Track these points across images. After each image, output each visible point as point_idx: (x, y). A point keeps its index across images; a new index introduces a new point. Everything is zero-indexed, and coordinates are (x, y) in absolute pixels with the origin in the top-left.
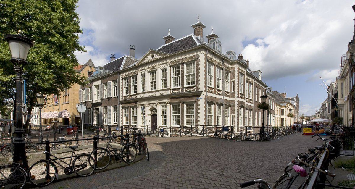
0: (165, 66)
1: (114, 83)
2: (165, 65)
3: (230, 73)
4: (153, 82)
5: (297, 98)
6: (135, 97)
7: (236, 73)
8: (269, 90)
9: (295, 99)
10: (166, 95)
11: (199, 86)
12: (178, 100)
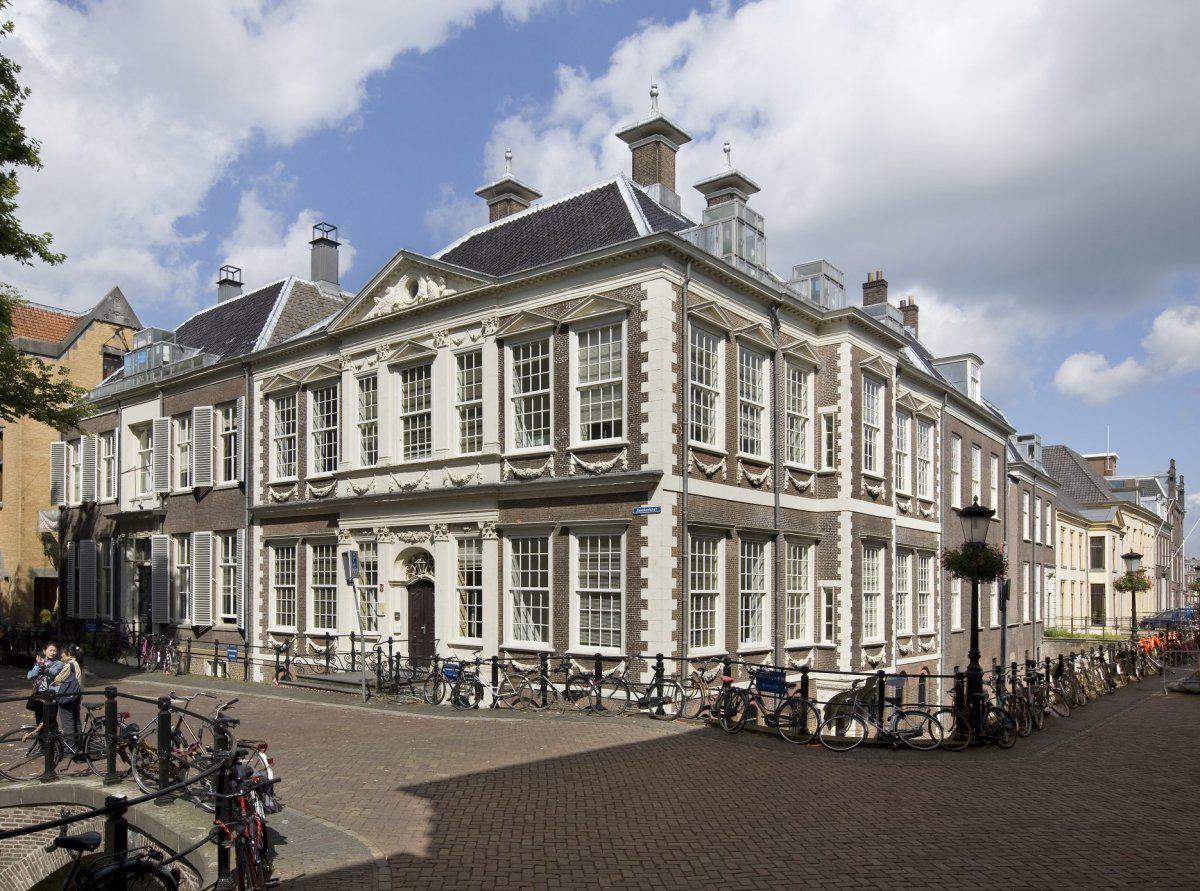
0: (473, 340)
1: (227, 416)
2: (477, 332)
3: (811, 377)
4: (414, 418)
5: (1172, 479)
6: (326, 489)
7: (845, 376)
8: (1022, 449)
9: (1161, 485)
10: (479, 488)
11: (645, 449)
12: (540, 516)
